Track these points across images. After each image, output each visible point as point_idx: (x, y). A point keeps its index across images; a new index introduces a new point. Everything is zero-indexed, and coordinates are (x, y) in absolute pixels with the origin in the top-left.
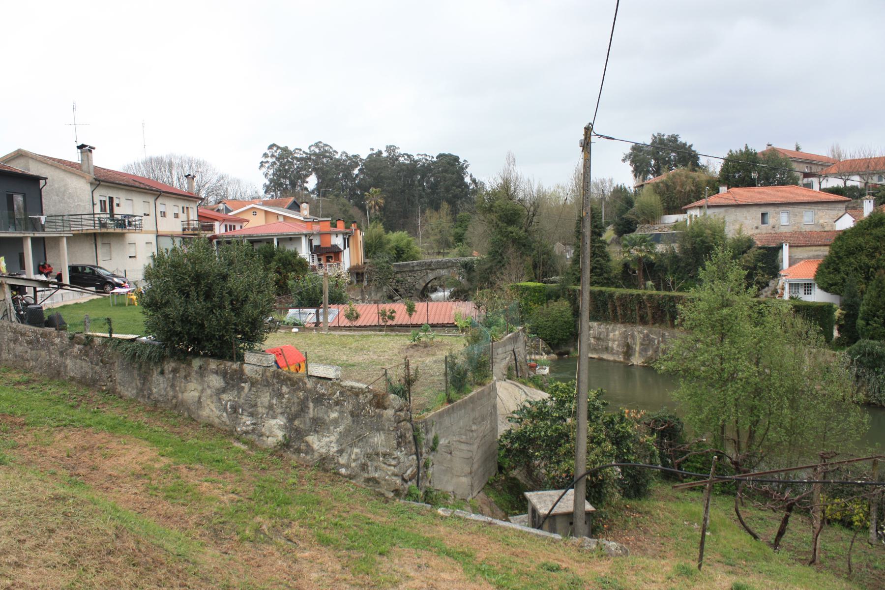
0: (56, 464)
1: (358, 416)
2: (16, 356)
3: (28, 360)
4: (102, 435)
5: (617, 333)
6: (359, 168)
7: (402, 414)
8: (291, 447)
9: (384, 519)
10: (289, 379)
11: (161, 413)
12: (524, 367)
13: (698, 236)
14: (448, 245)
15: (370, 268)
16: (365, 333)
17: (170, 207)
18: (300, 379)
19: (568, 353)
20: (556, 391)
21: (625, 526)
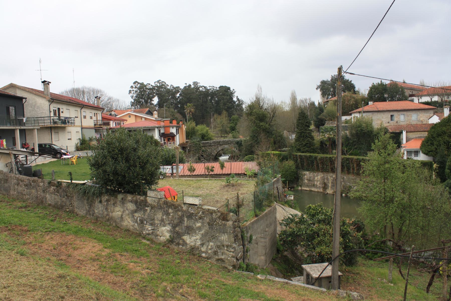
0: (49, 253)
1: (212, 225)
2: (18, 193)
3: (25, 195)
4: (70, 237)
5: (319, 177)
6: (179, 93)
7: (236, 224)
8: (174, 242)
9: (231, 282)
10: (173, 205)
11: (100, 223)
12: (282, 196)
13: (359, 127)
14: (226, 132)
16: (199, 179)
17: (88, 113)
18: (179, 205)
19: (294, 188)
20: (309, 209)
21: (348, 281)
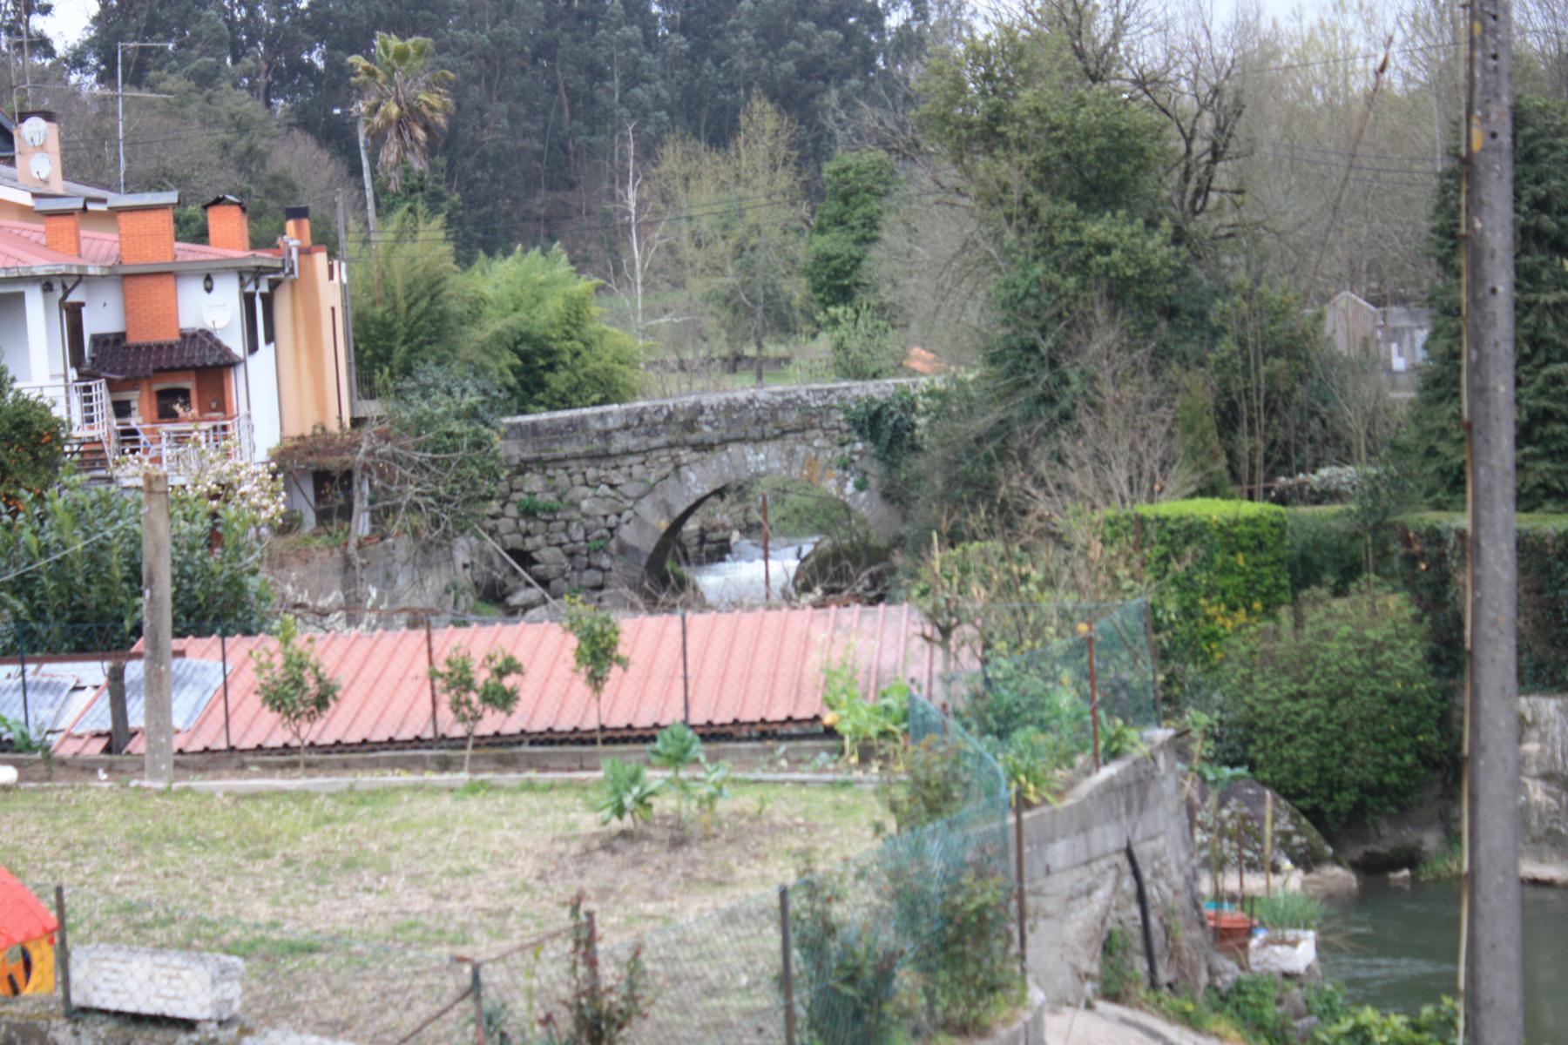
12: (1189, 936)
14: (782, 322)
15: (387, 448)
16: (367, 780)
19: (1411, 858)
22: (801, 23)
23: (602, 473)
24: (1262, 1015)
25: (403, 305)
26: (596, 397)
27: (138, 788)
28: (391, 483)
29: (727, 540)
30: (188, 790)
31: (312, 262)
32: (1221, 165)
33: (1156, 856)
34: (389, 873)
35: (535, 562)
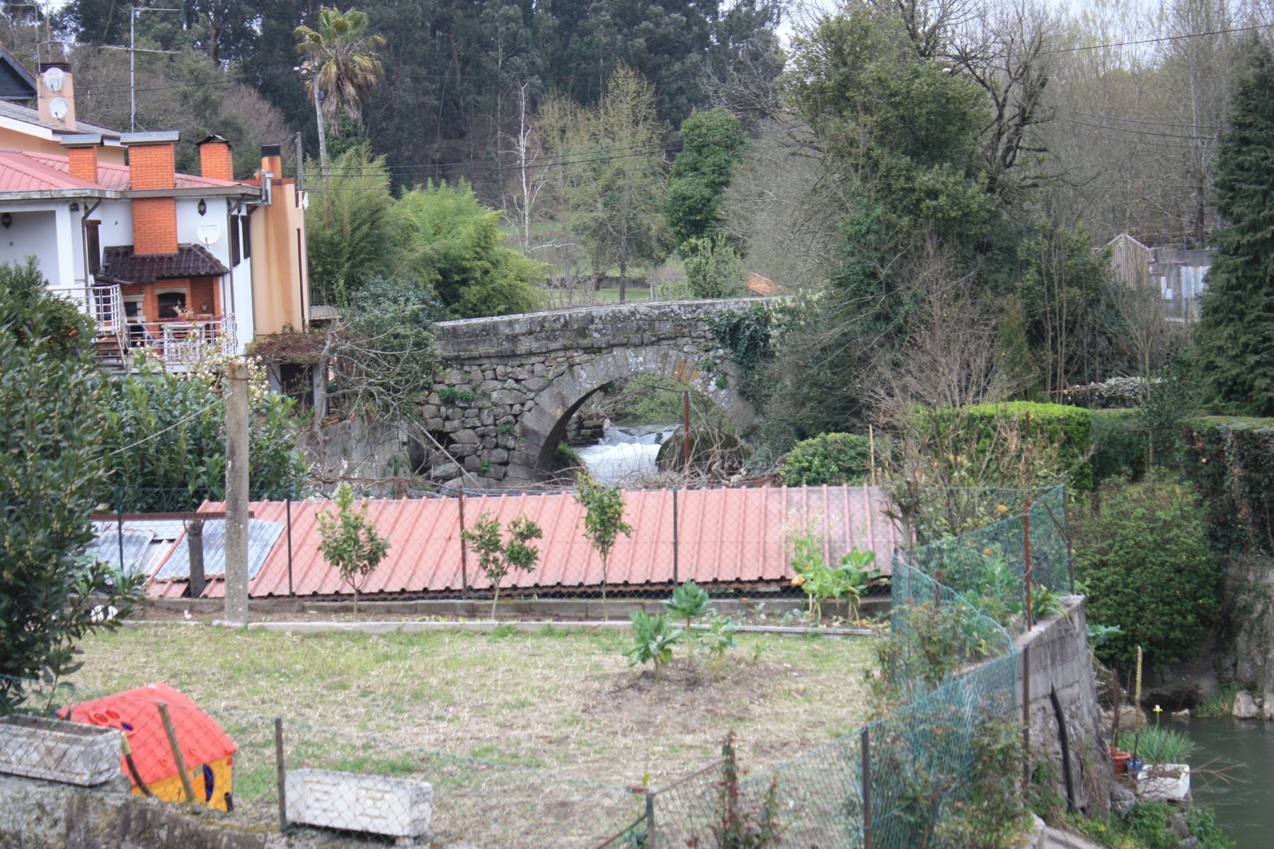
12: (1097, 768)
15: (347, 346)
16: (412, 623)
19: (1190, 700)
22: (652, 7)
23: (509, 370)
24: (1155, 835)
25: (348, 228)
26: (502, 308)
27: (218, 626)
28: (349, 374)
29: (600, 427)
30: (262, 629)
31: (282, 193)
32: (1027, 127)
33: (1072, 702)
34: (454, 704)
35: (453, 442)
